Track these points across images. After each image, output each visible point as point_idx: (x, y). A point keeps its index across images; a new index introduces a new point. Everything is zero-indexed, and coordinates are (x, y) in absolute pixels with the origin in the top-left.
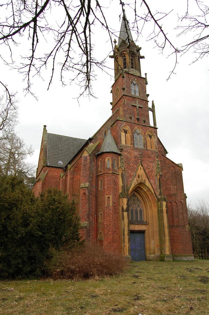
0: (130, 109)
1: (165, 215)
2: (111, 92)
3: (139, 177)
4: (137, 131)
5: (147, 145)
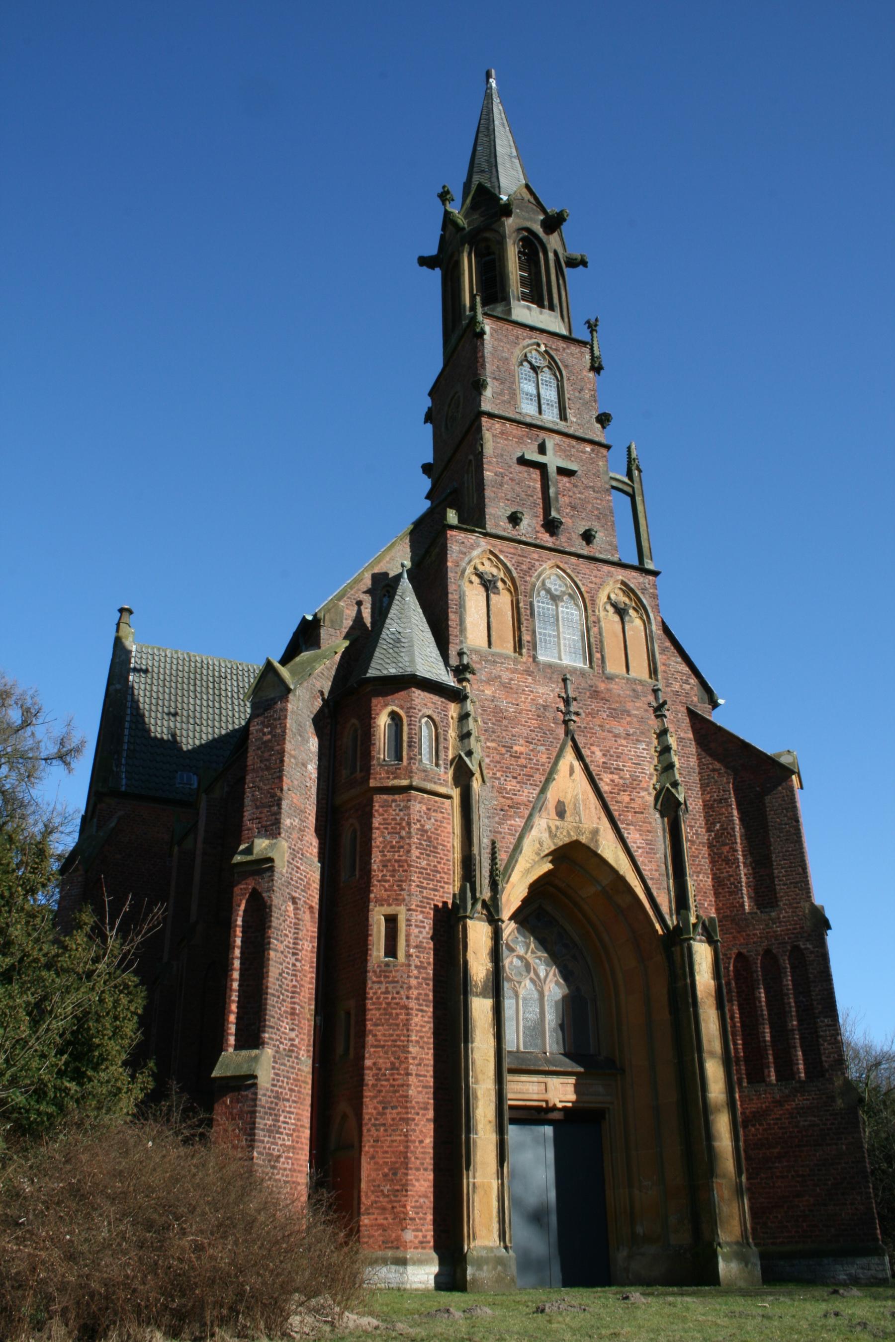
0: (512, 479)
1: (724, 987)
2: (429, 418)
3: (561, 813)
4: (548, 585)
5: (607, 656)
